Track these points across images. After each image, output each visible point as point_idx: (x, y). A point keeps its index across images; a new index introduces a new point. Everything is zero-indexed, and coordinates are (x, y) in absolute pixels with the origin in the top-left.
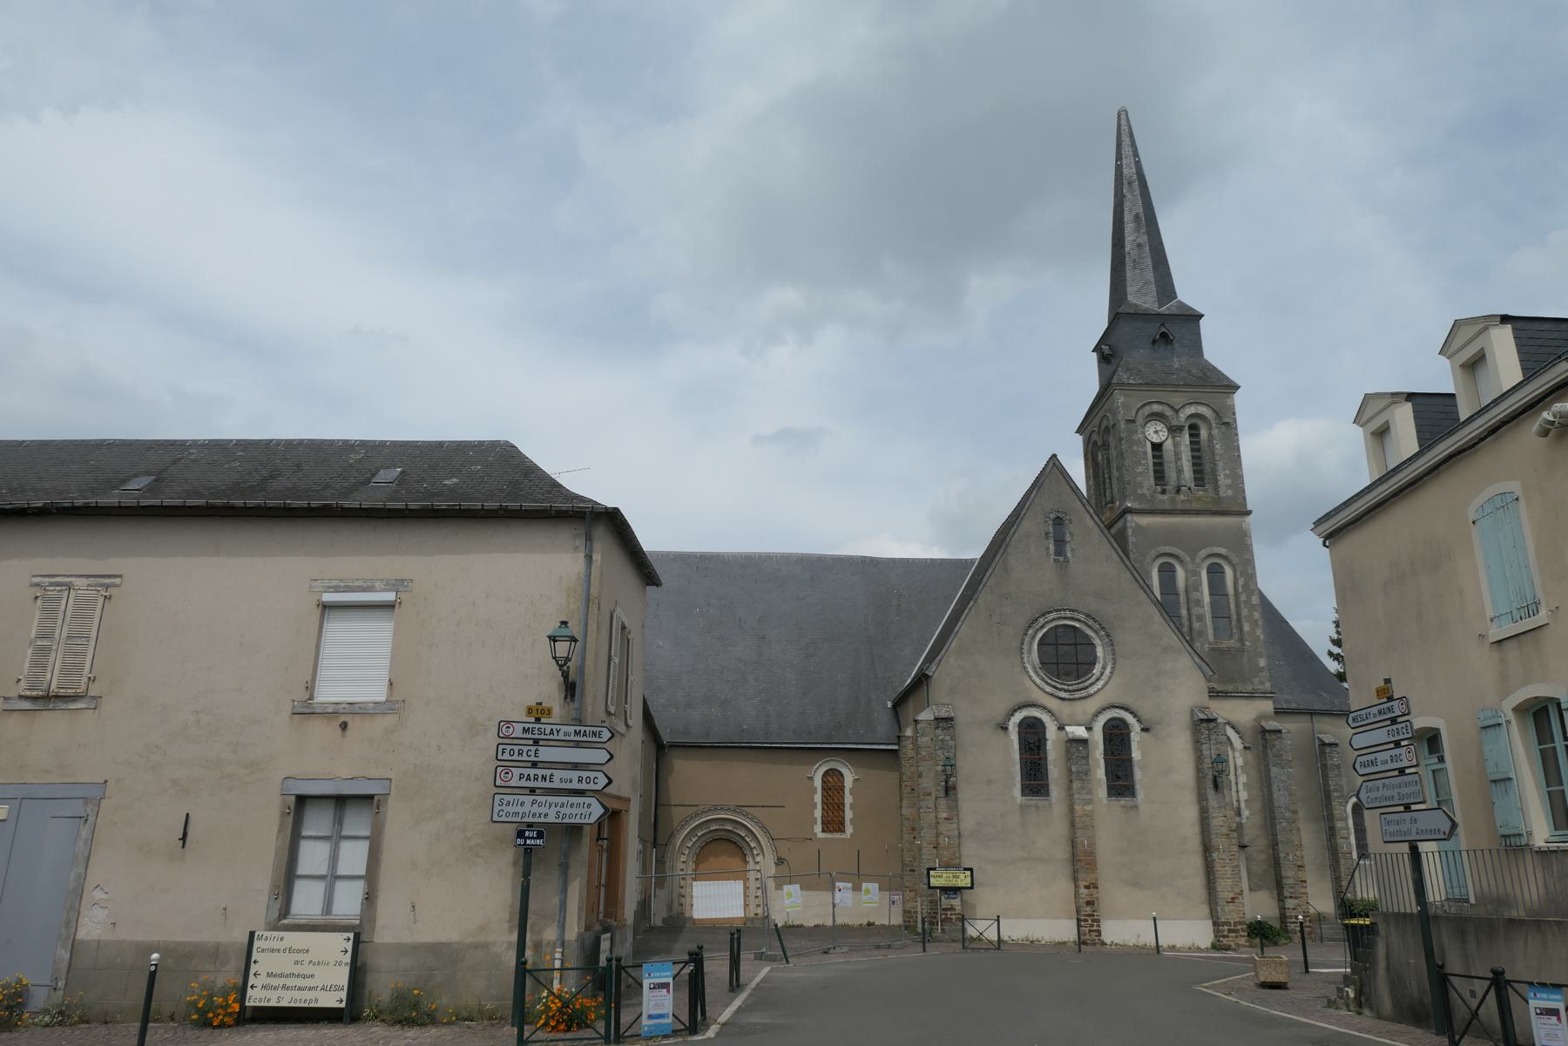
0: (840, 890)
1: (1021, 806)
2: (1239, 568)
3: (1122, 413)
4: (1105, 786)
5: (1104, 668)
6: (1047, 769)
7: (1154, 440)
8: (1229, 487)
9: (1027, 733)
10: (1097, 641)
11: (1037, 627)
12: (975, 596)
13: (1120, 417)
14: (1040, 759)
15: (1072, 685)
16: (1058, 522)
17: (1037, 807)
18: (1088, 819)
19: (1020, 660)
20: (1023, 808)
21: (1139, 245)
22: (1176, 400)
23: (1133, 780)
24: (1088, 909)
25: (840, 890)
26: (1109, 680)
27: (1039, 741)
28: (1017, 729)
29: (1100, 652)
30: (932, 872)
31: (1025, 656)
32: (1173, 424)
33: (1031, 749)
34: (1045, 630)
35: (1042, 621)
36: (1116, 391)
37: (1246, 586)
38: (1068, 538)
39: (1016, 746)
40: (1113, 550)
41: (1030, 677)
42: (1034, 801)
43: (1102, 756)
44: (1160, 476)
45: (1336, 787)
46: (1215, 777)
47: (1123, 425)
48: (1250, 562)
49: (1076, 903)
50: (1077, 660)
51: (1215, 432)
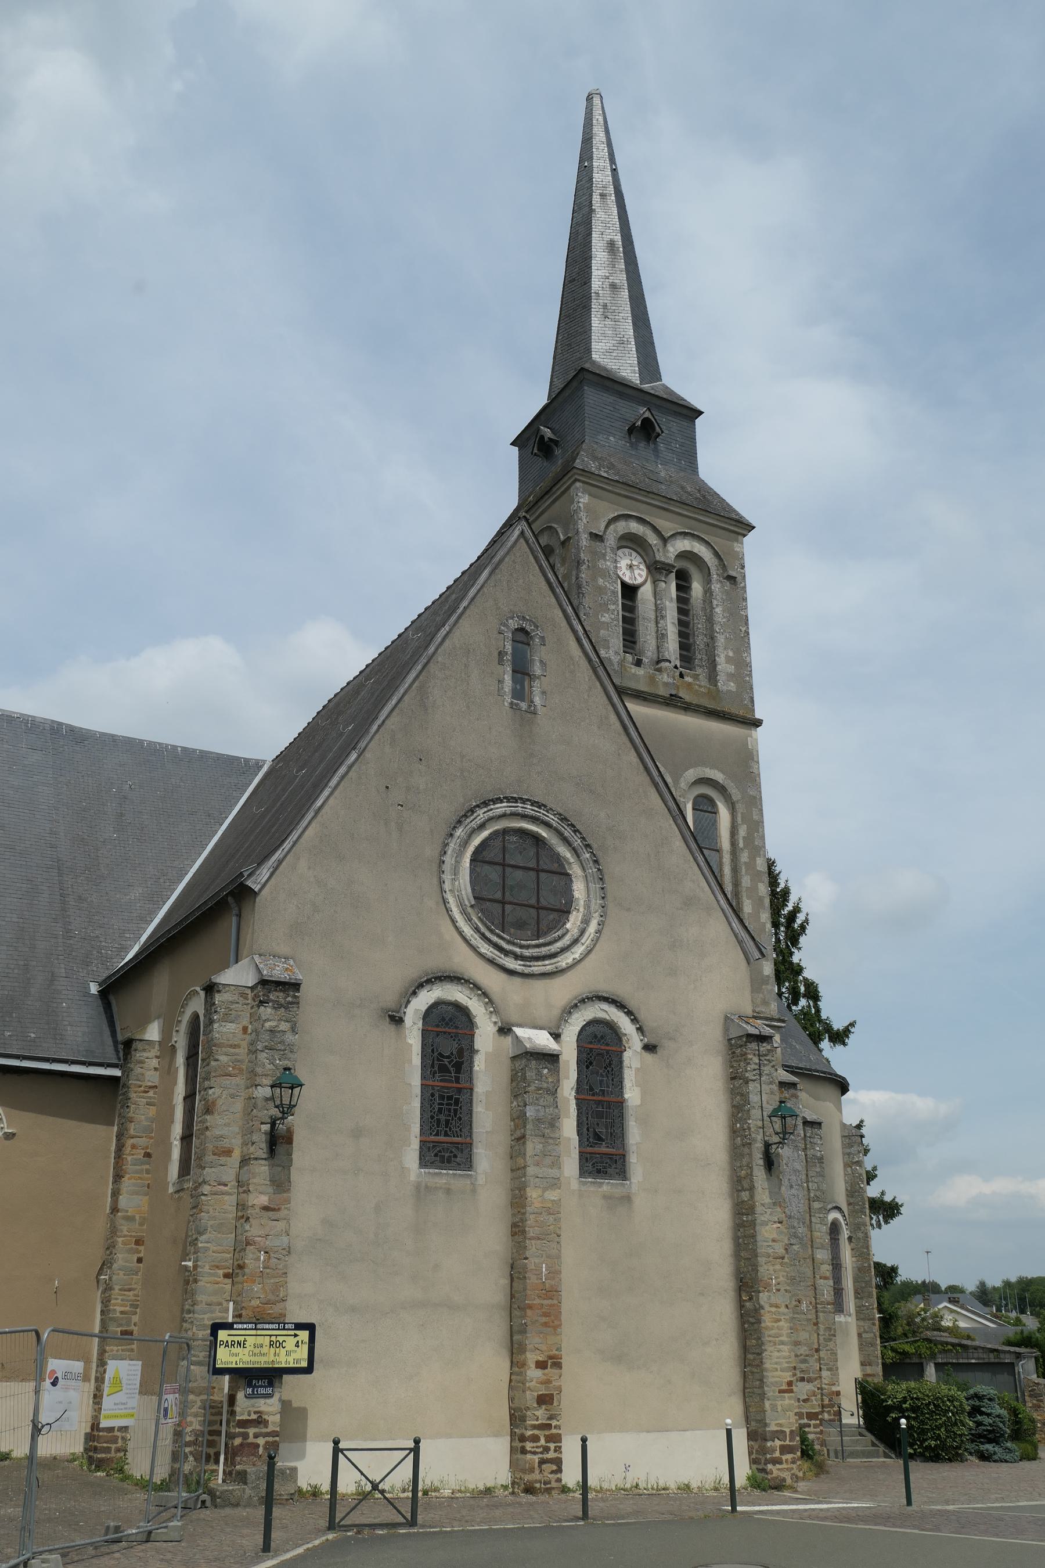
0: (54, 1384)
1: (418, 1187)
2: (740, 808)
3: (585, 521)
4: (575, 1155)
5: (586, 921)
6: (470, 1112)
7: (627, 579)
8: (731, 676)
9: (438, 1034)
10: (575, 870)
11: (474, 825)
12: (362, 745)
13: (581, 526)
14: (459, 1091)
15: (528, 947)
16: (523, 636)
17: (448, 1191)
18: (551, 1218)
19: (435, 881)
20: (422, 1192)
21: (613, 286)
22: (667, 526)
23: (623, 1145)
24: (541, 1413)
25: (54, 1384)
26: (595, 945)
27: (461, 1052)
28: (420, 1024)
29: (579, 889)
30: (222, 1335)
31: (447, 877)
32: (658, 558)
33: (443, 1069)
34: (485, 834)
35: (481, 815)
36: (578, 484)
37: (749, 840)
38: (537, 670)
39: (417, 1060)
40: (610, 708)
41: (453, 921)
42: (444, 1177)
43: (573, 1093)
44: (630, 638)
45: (818, 1193)
46: (767, 1146)
47: (584, 540)
48: (755, 802)
49: (511, 1399)
50: (538, 901)
51: (716, 587)
